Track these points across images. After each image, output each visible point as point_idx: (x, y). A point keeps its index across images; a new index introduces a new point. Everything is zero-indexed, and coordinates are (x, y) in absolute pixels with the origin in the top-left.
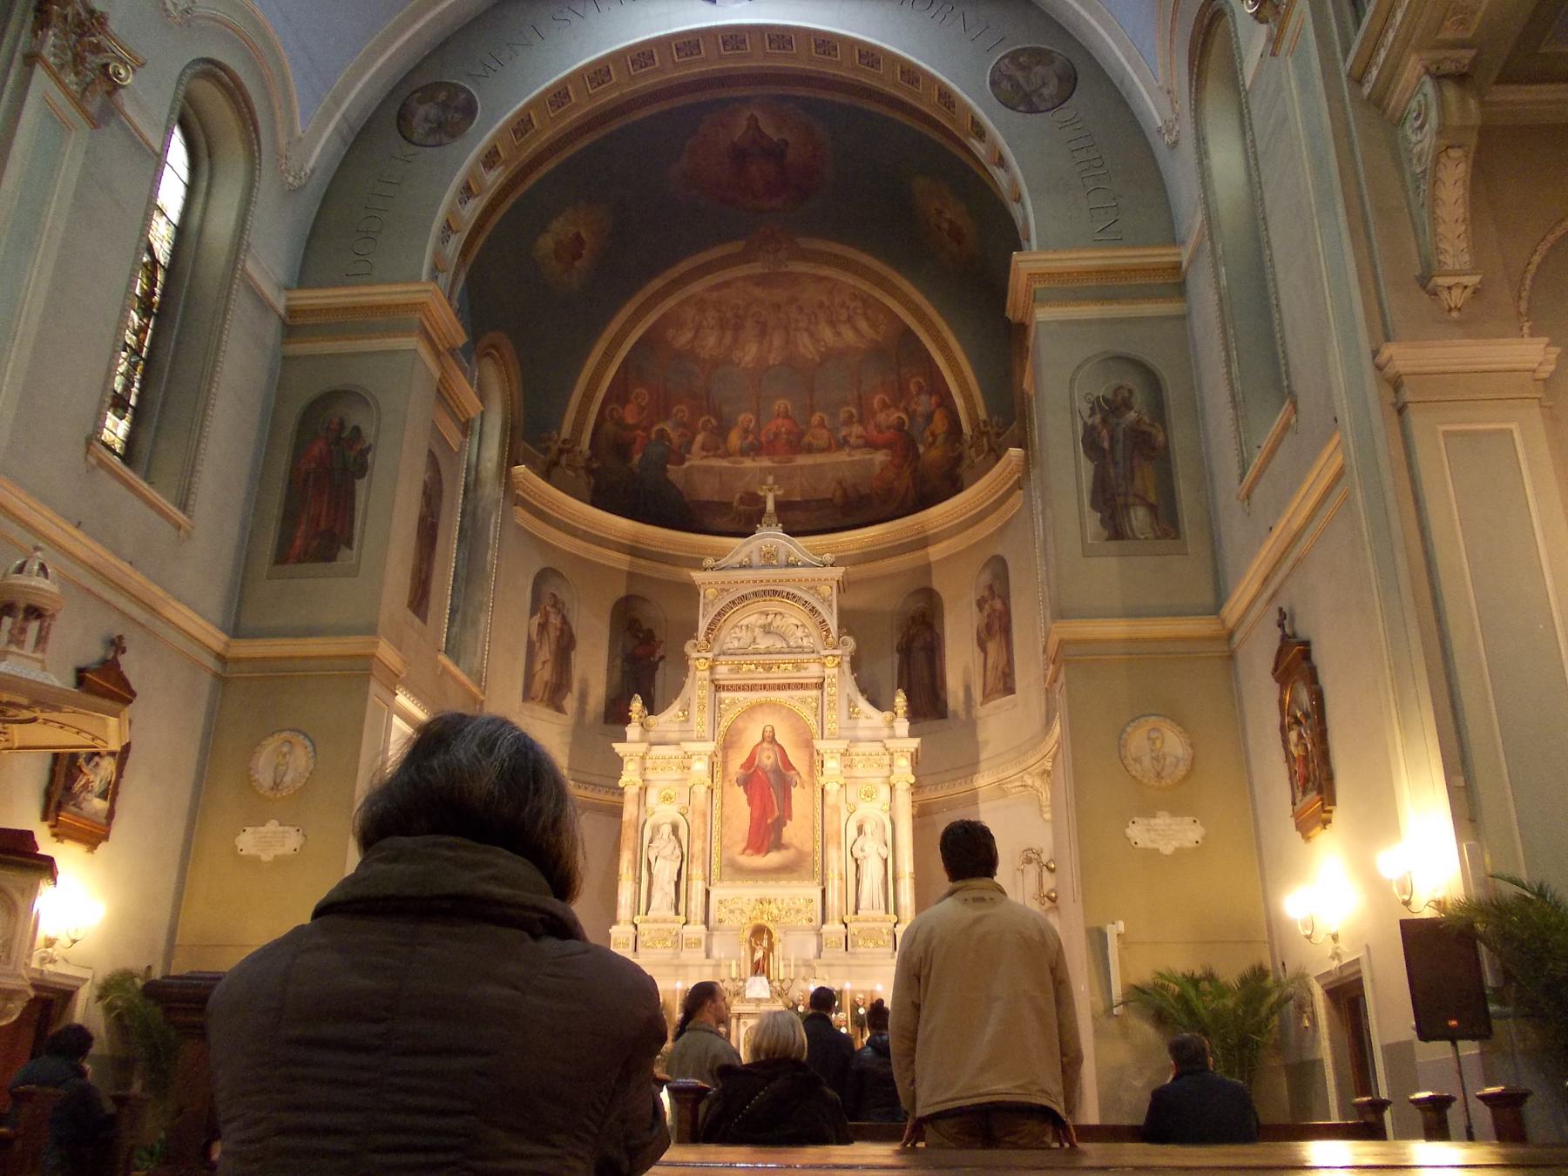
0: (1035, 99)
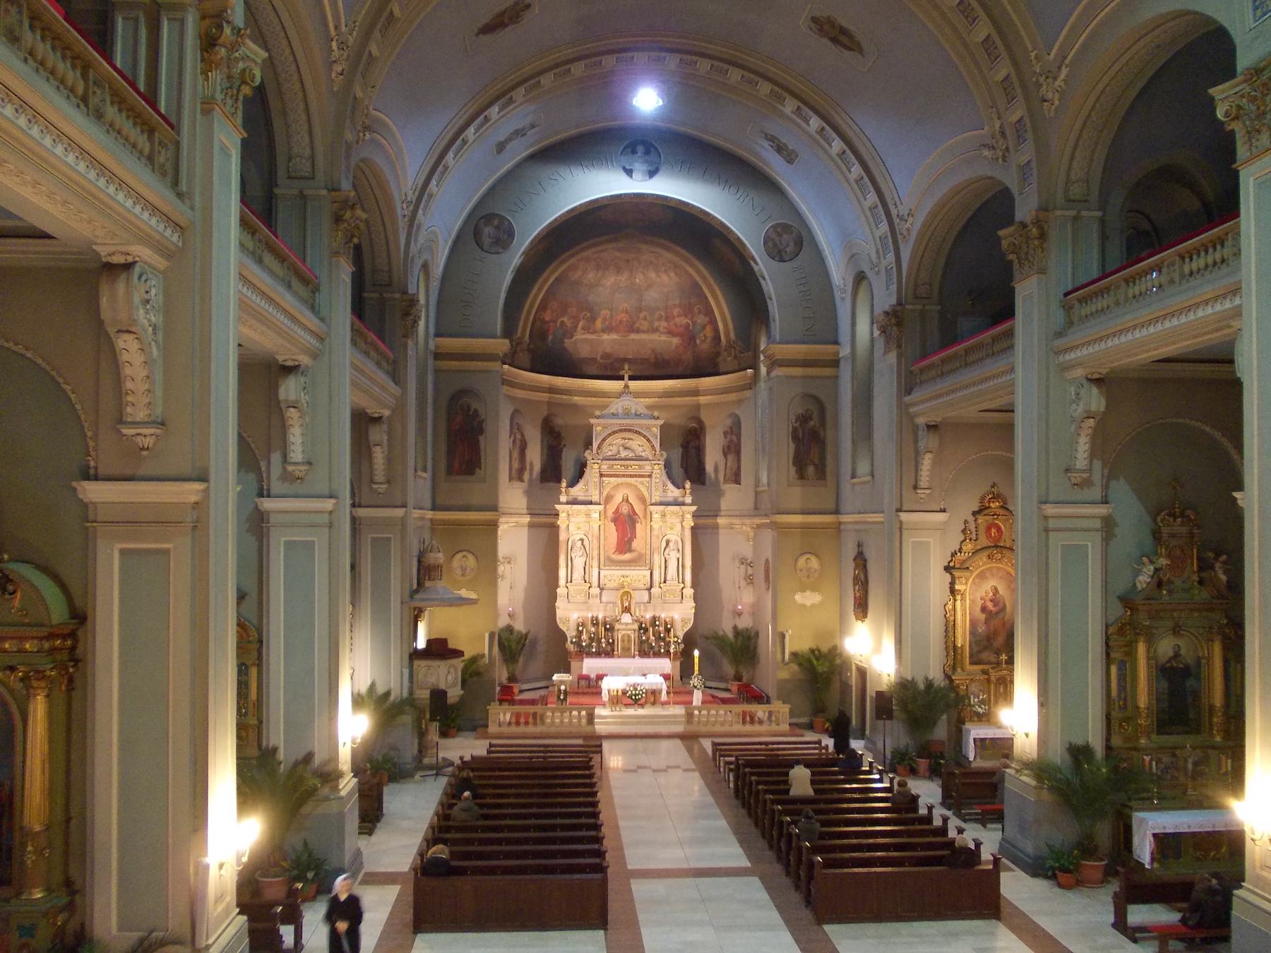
0: (783, 254)
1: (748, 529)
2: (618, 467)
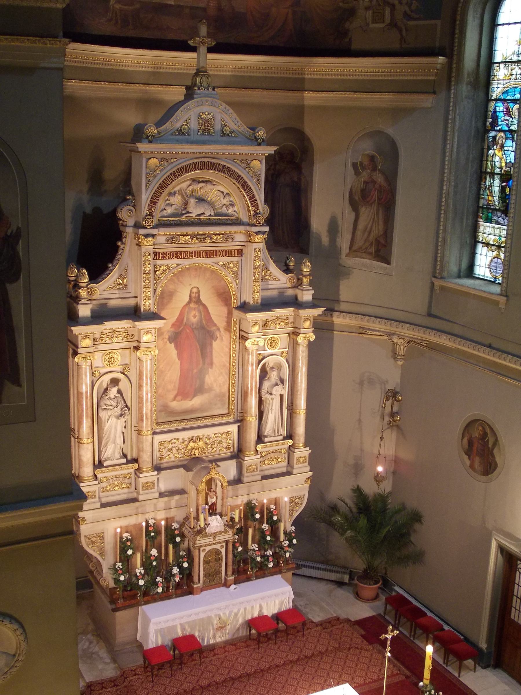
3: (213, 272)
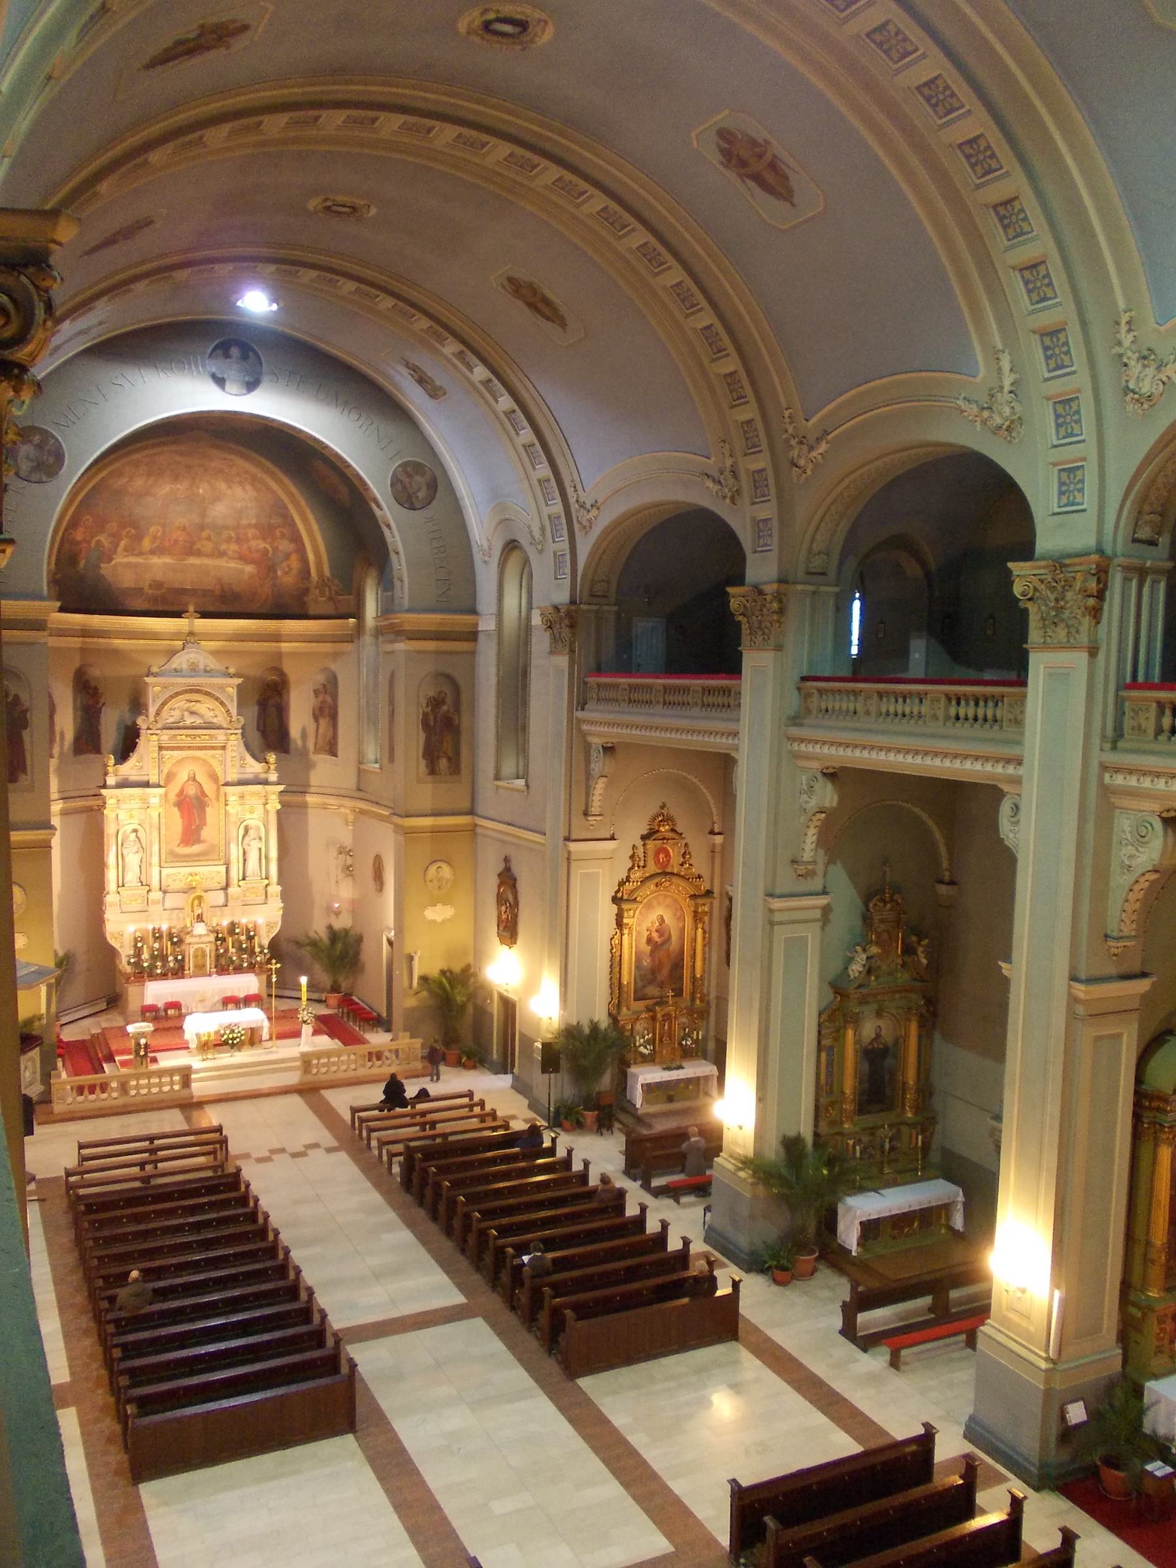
0: (414, 500)
1: (348, 811)
2: (183, 737)
3: (204, 760)
